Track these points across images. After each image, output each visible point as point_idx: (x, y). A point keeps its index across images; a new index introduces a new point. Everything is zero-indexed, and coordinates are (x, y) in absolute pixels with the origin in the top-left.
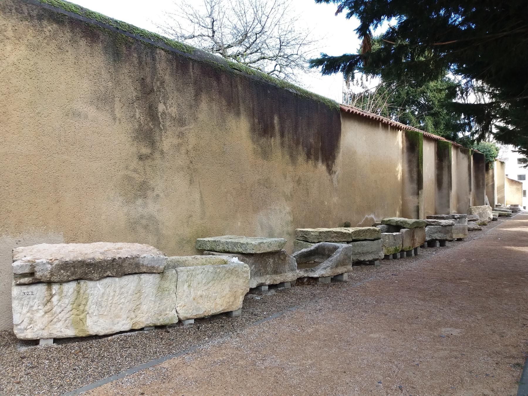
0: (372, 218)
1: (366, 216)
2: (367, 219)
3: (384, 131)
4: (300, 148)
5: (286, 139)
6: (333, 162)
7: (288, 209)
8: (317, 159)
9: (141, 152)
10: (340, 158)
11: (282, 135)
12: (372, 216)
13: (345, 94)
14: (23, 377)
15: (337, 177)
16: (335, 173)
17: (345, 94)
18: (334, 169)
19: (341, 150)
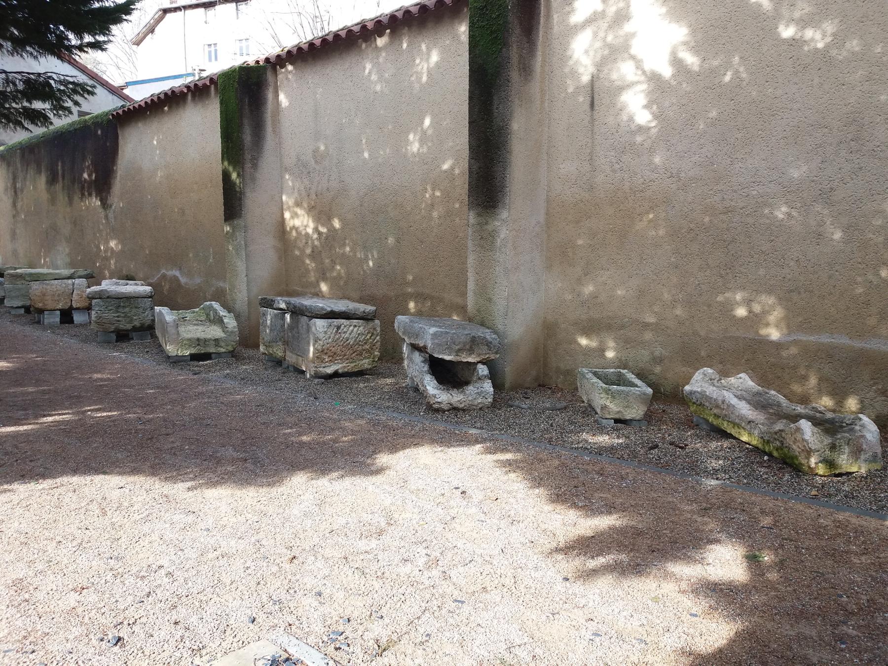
0: (176, 279)
1: (163, 271)
2: (164, 276)
3: (200, 106)
4: (76, 186)
5: (66, 181)
6: (109, 192)
7: (67, 250)
8: (90, 195)
9: (828, 440)
10: (117, 187)
11: (63, 178)
12: (177, 273)
13: (299, 160)
14: (656, 446)
15: (114, 212)
16: (111, 206)
17: (299, 160)
18: (109, 202)
19: (118, 175)
